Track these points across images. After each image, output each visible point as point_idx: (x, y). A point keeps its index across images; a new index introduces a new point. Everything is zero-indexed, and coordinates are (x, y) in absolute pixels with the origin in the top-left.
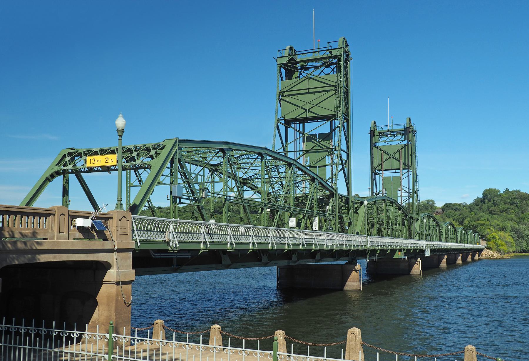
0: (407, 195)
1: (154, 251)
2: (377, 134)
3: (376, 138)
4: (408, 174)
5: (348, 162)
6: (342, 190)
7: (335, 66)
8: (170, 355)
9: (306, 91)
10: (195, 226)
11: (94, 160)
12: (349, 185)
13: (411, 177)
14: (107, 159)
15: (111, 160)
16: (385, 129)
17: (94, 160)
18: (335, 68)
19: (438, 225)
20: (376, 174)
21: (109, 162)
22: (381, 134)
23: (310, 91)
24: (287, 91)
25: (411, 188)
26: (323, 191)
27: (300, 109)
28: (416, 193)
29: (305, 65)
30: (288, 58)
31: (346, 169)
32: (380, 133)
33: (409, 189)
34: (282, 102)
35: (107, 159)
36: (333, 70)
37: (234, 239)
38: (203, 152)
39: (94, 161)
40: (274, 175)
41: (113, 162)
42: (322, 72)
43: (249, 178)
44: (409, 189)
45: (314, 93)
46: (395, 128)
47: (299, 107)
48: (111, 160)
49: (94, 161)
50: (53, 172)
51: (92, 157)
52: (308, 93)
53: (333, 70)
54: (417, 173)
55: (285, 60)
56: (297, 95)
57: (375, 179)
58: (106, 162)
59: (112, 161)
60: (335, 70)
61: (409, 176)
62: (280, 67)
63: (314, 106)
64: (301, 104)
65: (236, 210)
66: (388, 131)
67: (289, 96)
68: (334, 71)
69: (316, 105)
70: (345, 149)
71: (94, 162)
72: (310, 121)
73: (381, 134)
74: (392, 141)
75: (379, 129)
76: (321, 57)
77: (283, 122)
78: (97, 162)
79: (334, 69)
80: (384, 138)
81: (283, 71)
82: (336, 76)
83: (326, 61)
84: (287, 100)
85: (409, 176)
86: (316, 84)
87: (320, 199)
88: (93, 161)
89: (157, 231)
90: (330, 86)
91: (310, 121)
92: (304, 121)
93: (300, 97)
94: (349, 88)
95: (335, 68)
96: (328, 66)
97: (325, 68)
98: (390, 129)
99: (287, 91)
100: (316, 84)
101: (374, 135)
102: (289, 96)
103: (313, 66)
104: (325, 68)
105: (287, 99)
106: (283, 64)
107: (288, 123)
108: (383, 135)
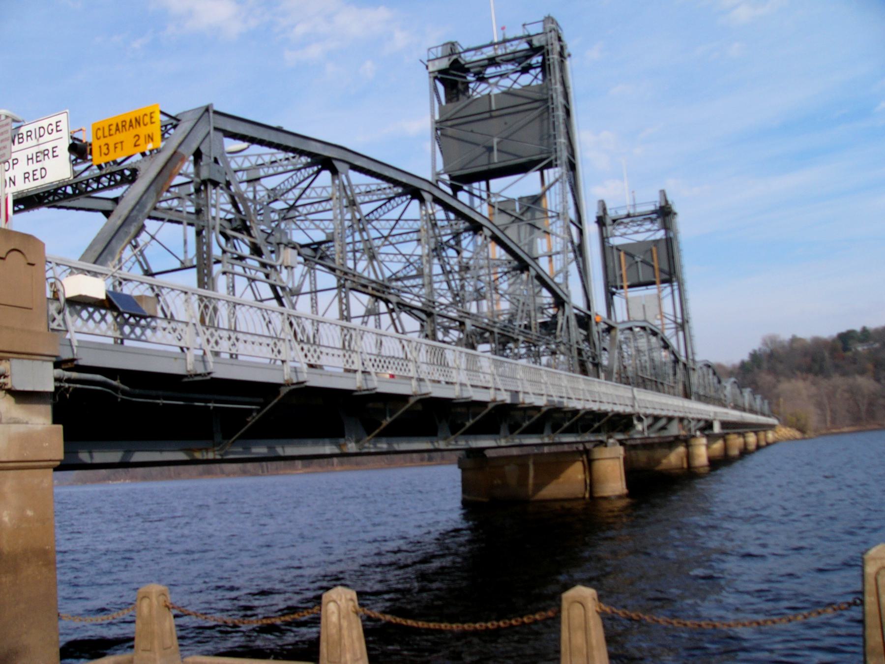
2: (608, 221)
3: (610, 228)
6: (577, 299)
8: (581, 342)
9: (487, 115)
13: (676, 293)
15: (10, 179)
16: (623, 213)
20: (613, 294)
32: (614, 221)
38: (436, 286)
40: (240, 163)
41: (14, 183)
46: (640, 210)
66: (628, 216)
72: (455, 73)
74: (637, 232)
75: (611, 214)
77: (446, 177)
79: (537, 75)
80: (621, 230)
81: (441, 88)
89: (434, 364)
91: (455, 73)
92: (487, 175)
96: (525, 71)
98: (632, 211)
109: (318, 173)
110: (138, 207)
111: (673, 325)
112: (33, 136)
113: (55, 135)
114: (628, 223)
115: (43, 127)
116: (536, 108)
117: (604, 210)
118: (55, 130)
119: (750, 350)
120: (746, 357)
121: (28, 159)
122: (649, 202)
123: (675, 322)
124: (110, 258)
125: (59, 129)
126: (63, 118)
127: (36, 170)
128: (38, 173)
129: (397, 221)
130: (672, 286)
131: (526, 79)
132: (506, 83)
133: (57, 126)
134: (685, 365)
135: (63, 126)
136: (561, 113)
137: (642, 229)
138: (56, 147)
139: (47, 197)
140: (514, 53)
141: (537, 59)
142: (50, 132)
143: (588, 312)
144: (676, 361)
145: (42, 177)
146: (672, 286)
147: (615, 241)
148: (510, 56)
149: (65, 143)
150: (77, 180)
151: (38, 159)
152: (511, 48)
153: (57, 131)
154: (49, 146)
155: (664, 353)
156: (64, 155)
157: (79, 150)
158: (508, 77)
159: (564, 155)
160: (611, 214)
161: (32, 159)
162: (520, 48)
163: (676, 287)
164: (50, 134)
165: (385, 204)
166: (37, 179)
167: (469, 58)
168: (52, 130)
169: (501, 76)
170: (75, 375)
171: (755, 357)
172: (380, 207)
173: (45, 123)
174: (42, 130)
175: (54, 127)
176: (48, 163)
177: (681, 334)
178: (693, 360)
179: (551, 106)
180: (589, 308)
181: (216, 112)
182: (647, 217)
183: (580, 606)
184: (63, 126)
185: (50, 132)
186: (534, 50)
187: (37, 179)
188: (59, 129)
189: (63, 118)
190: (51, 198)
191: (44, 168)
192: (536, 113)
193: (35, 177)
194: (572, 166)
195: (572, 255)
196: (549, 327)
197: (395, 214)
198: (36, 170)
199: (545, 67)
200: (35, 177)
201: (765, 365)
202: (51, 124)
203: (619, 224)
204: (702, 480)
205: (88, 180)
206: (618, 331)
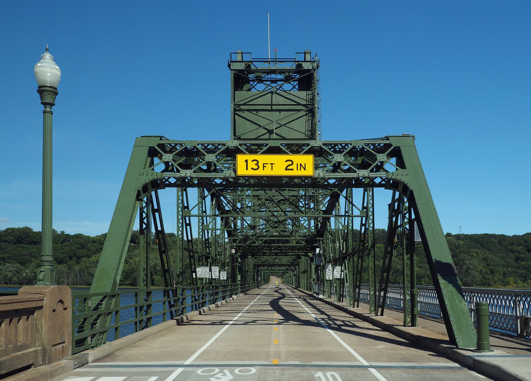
1: (441, 362)
9: (269, 108)
10: (427, 298)
11: (256, 162)
14: (291, 163)
15: (301, 165)
17: (256, 162)
21: (295, 168)
23: (274, 107)
24: (245, 104)
27: (261, 128)
30: (246, 64)
34: (236, 117)
35: (291, 163)
39: (257, 164)
41: (305, 169)
45: (280, 111)
47: (260, 126)
48: (301, 165)
49: (257, 164)
50: (147, 181)
51: (250, 157)
52: (272, 110)
56: (257, 110)
58: (286, 169)
59: (303, 167)
60: (297, 87)
63: (281, 126)
64: (263, 122)
65: (10, 240)
67: (249, 111)
69: (284, 125)
71: (256, 167)
76: (289, 69)
78: (264, 167)
82: (307, 95)
83: (289, 75)
84: (244, 115)
86: (282, 100)
87: (513, 253)
88: (252, 165)
90: (299, 104)
93: (260, 113)
99: (245, 104)
100: (282, 100)
102: (249, 111)
103: (268, 79)
105: (246, 114)
106: (238, 70)
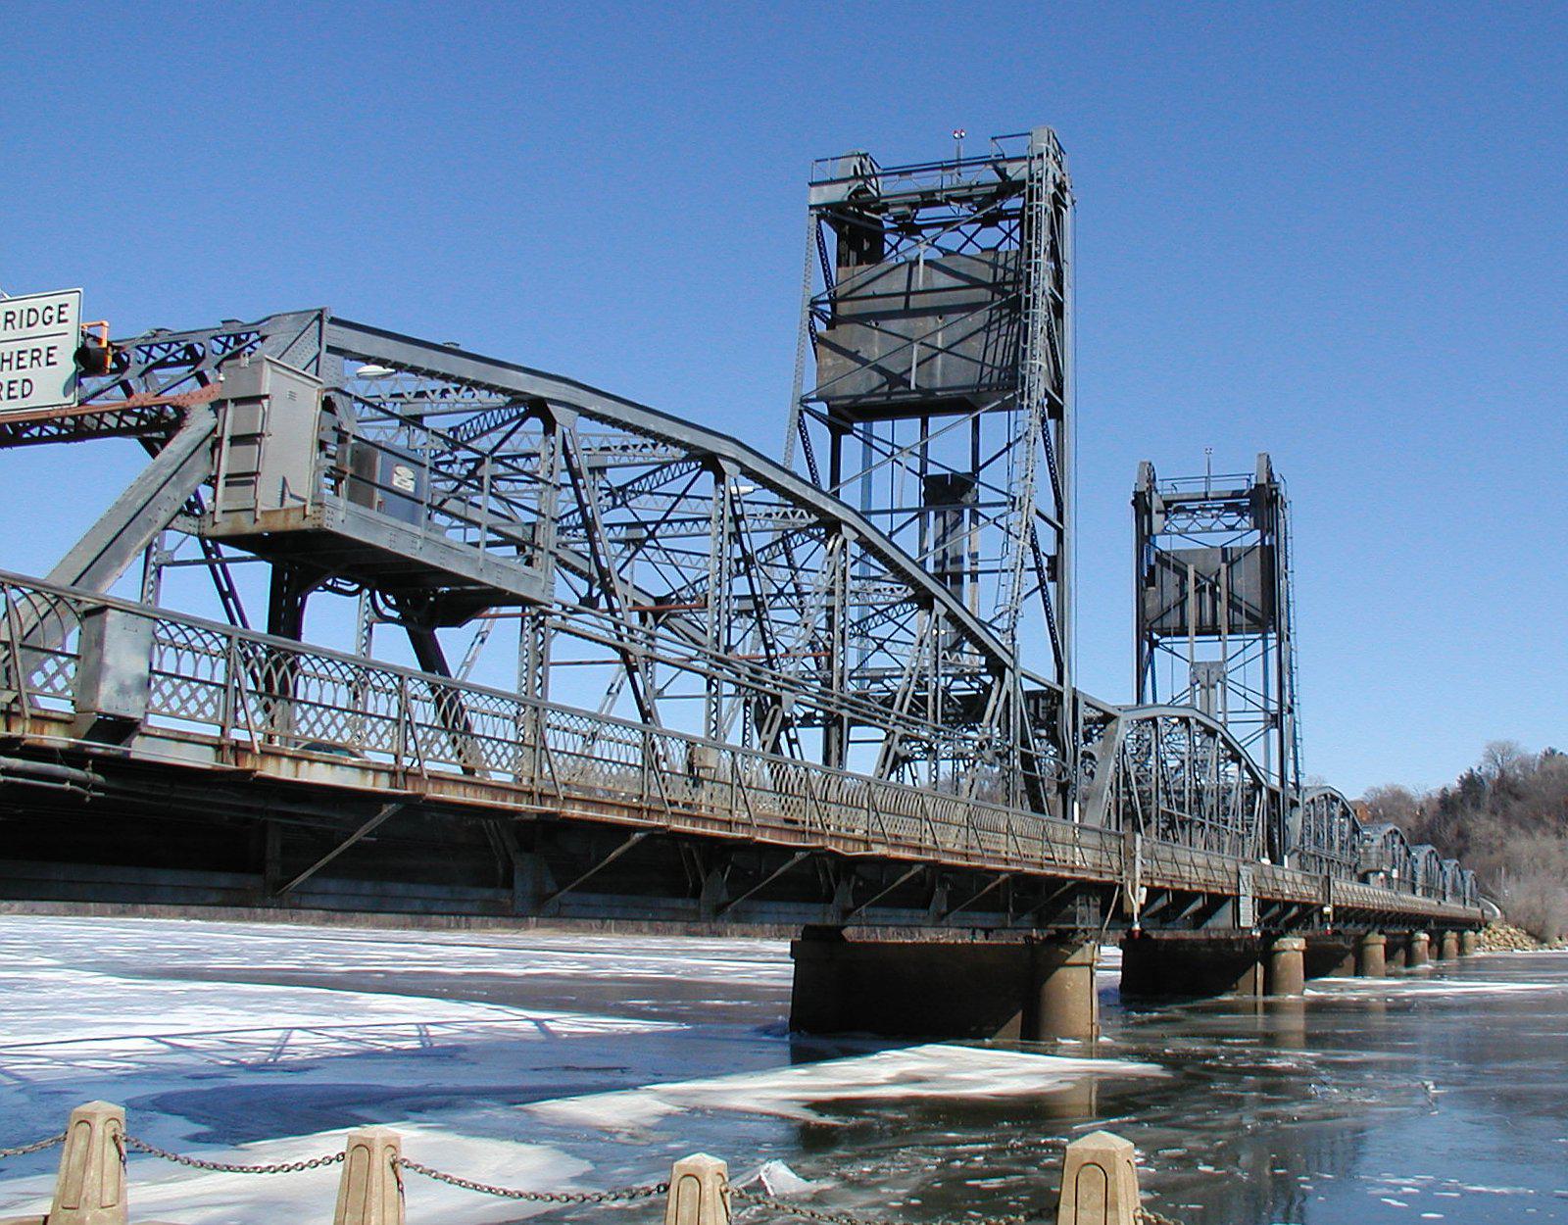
0: (1262, 719)
2: (1157, 503)
4: (1265, 644)
5: (1054, 568)
6: (1035, 661)
7: (1015, 222)
12: (1063, 483)
13: (1273, 654)
18: (1015, 228)
19: (1356, 830)
20: (1154, 644)
22: (1170, 507)
25: (1274, 694)
26: (794, 513)
28: (1291, 711)
29: (908, 216)
31: (1051, 586)
32: (1168, 504)
33: (1266, 697)
36: (1008, 235)
37: (783, 808)
42: (970, 243)
43: (674, 597)
44: (1266, 697)
53: (1008, 235)
54: (1292, 641)
55: (839, 193)
57: (1151, 661)
60: (1016, 234)
61: (1265, 651)
62: (819, 218)
68: (1011, 238)
70: (1052, 515)
73: (1170, 507)
74: (1210, 530)
75: (1164, 490)
77: (822, 408)
79: (1012, 231)
80: (1181, 521)
81: (831, 237)
85: (1265, 651)
94: (1065, 523)
95: (1015, 228)
96: (989, 221)
97: (979, 229)
101: (1149, 512)
104: (979, 229)
107: (840, 420)
108: (1181, 510)
109: (524, 418)
110: (174, 478)
111: (1261, 716)
112: (16, 322)
113: (56, 327)
114: (1194, 511)
115: (35, 310)
116: (972, 308)
117: (1152, 480)
118: (55, 319)
119: (1464, 772)
120: (1454, 784)
121: (3, 361)
122: (1237, 474)
123: (1266, 711)
124: (116, 563)
125: (62, 317)
126: (72, 299)
127: (15, 382)
128: (17, 387)
129: (679, 497)
130: (1265, 640)
131: (990, 236)
132: (951, 240)
133: (60, 313)
134: (1273, 794)
135: (70, 313)
136: (1041, 312)
137: (1219, 526)
138: (54, 348)
139: (27, 430)
140: (970, 188)
141: (1014, 203)
142: (47, 320)
143: (1058, 688)
144: (1257, 786)
145: (24, 396)
146: (1265, 640)
147: (1163, 543)
148: (965, 193)
149: (67, 349)
150: (83, 410)
151: (21, 364)
152: (970, 176)
153: (59, 321)
154: (43, 344)
155: (1233, 768)
156: (67, 366)
157: (88, 360)
158: (958, 229)
159: (1039, 387)
160: (1164, 490)
161: (10, 361)
162: (983, 179)
163: (1272, 643)
164: (46, 323)
165: (654, 472)
166: (15, 397)
167: (885, 187)
168: (51, 317)
169: (945, 225)
170: (17, 763)
171: (1471, 784)
172: (646, 476)
173: (40, 304)
174: (33, 314)
175: (55, 313)
176: (38, 373)
177: (1274, 733)
178: (1297, 785)
179: (1025, 295)
180: (1060, 680)
181: (334, 321)
182: (1232, 504)
183: (687, 1179)
184: (70, 313)
185: (47, 320)
186: (1009, 188)
187: (15, 397)
188: (62, 317)
189: (72, 299)
190: (35, 432)
191: (28, 381)
192: (980, 318)
193: (12, 393)
194: (1056, 411)
195: (1033, 579)
196: (971, 710)
197: (677, 487)
198: (15, 382)
199: (1025, 220)
200: (12, 393)
201: (1487, 801)
202: (50, 308)
203: (1177, 511)
204: (1289, 1017)
205: (102, 414)
206: (1121, 723)
